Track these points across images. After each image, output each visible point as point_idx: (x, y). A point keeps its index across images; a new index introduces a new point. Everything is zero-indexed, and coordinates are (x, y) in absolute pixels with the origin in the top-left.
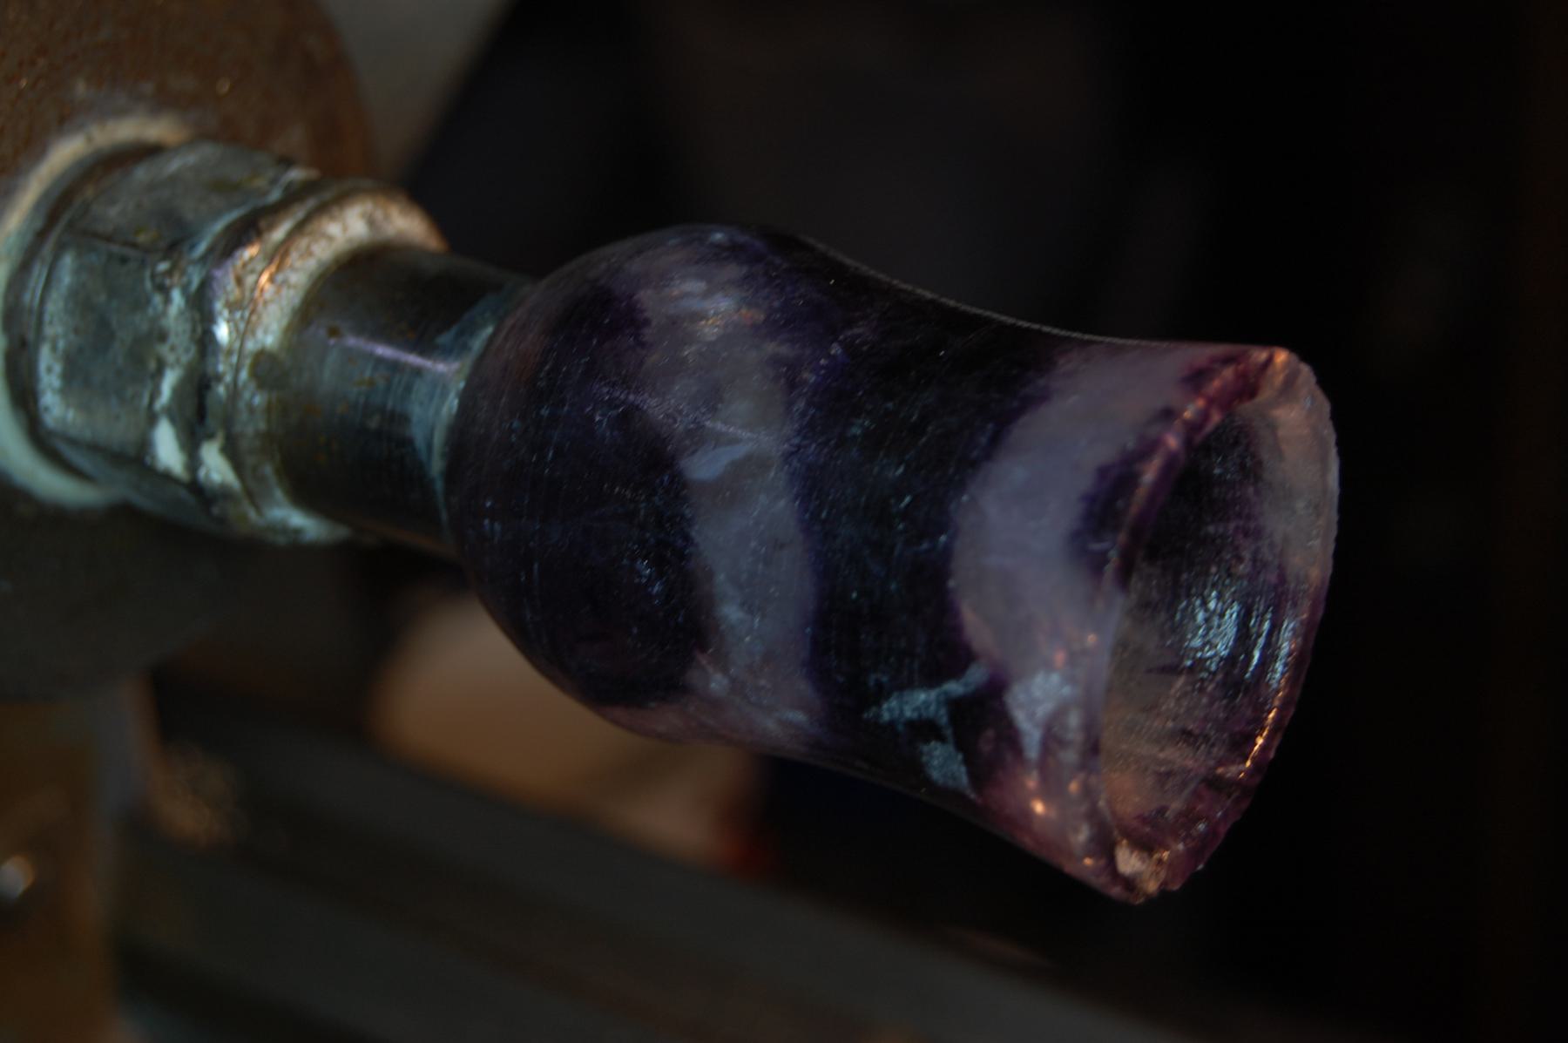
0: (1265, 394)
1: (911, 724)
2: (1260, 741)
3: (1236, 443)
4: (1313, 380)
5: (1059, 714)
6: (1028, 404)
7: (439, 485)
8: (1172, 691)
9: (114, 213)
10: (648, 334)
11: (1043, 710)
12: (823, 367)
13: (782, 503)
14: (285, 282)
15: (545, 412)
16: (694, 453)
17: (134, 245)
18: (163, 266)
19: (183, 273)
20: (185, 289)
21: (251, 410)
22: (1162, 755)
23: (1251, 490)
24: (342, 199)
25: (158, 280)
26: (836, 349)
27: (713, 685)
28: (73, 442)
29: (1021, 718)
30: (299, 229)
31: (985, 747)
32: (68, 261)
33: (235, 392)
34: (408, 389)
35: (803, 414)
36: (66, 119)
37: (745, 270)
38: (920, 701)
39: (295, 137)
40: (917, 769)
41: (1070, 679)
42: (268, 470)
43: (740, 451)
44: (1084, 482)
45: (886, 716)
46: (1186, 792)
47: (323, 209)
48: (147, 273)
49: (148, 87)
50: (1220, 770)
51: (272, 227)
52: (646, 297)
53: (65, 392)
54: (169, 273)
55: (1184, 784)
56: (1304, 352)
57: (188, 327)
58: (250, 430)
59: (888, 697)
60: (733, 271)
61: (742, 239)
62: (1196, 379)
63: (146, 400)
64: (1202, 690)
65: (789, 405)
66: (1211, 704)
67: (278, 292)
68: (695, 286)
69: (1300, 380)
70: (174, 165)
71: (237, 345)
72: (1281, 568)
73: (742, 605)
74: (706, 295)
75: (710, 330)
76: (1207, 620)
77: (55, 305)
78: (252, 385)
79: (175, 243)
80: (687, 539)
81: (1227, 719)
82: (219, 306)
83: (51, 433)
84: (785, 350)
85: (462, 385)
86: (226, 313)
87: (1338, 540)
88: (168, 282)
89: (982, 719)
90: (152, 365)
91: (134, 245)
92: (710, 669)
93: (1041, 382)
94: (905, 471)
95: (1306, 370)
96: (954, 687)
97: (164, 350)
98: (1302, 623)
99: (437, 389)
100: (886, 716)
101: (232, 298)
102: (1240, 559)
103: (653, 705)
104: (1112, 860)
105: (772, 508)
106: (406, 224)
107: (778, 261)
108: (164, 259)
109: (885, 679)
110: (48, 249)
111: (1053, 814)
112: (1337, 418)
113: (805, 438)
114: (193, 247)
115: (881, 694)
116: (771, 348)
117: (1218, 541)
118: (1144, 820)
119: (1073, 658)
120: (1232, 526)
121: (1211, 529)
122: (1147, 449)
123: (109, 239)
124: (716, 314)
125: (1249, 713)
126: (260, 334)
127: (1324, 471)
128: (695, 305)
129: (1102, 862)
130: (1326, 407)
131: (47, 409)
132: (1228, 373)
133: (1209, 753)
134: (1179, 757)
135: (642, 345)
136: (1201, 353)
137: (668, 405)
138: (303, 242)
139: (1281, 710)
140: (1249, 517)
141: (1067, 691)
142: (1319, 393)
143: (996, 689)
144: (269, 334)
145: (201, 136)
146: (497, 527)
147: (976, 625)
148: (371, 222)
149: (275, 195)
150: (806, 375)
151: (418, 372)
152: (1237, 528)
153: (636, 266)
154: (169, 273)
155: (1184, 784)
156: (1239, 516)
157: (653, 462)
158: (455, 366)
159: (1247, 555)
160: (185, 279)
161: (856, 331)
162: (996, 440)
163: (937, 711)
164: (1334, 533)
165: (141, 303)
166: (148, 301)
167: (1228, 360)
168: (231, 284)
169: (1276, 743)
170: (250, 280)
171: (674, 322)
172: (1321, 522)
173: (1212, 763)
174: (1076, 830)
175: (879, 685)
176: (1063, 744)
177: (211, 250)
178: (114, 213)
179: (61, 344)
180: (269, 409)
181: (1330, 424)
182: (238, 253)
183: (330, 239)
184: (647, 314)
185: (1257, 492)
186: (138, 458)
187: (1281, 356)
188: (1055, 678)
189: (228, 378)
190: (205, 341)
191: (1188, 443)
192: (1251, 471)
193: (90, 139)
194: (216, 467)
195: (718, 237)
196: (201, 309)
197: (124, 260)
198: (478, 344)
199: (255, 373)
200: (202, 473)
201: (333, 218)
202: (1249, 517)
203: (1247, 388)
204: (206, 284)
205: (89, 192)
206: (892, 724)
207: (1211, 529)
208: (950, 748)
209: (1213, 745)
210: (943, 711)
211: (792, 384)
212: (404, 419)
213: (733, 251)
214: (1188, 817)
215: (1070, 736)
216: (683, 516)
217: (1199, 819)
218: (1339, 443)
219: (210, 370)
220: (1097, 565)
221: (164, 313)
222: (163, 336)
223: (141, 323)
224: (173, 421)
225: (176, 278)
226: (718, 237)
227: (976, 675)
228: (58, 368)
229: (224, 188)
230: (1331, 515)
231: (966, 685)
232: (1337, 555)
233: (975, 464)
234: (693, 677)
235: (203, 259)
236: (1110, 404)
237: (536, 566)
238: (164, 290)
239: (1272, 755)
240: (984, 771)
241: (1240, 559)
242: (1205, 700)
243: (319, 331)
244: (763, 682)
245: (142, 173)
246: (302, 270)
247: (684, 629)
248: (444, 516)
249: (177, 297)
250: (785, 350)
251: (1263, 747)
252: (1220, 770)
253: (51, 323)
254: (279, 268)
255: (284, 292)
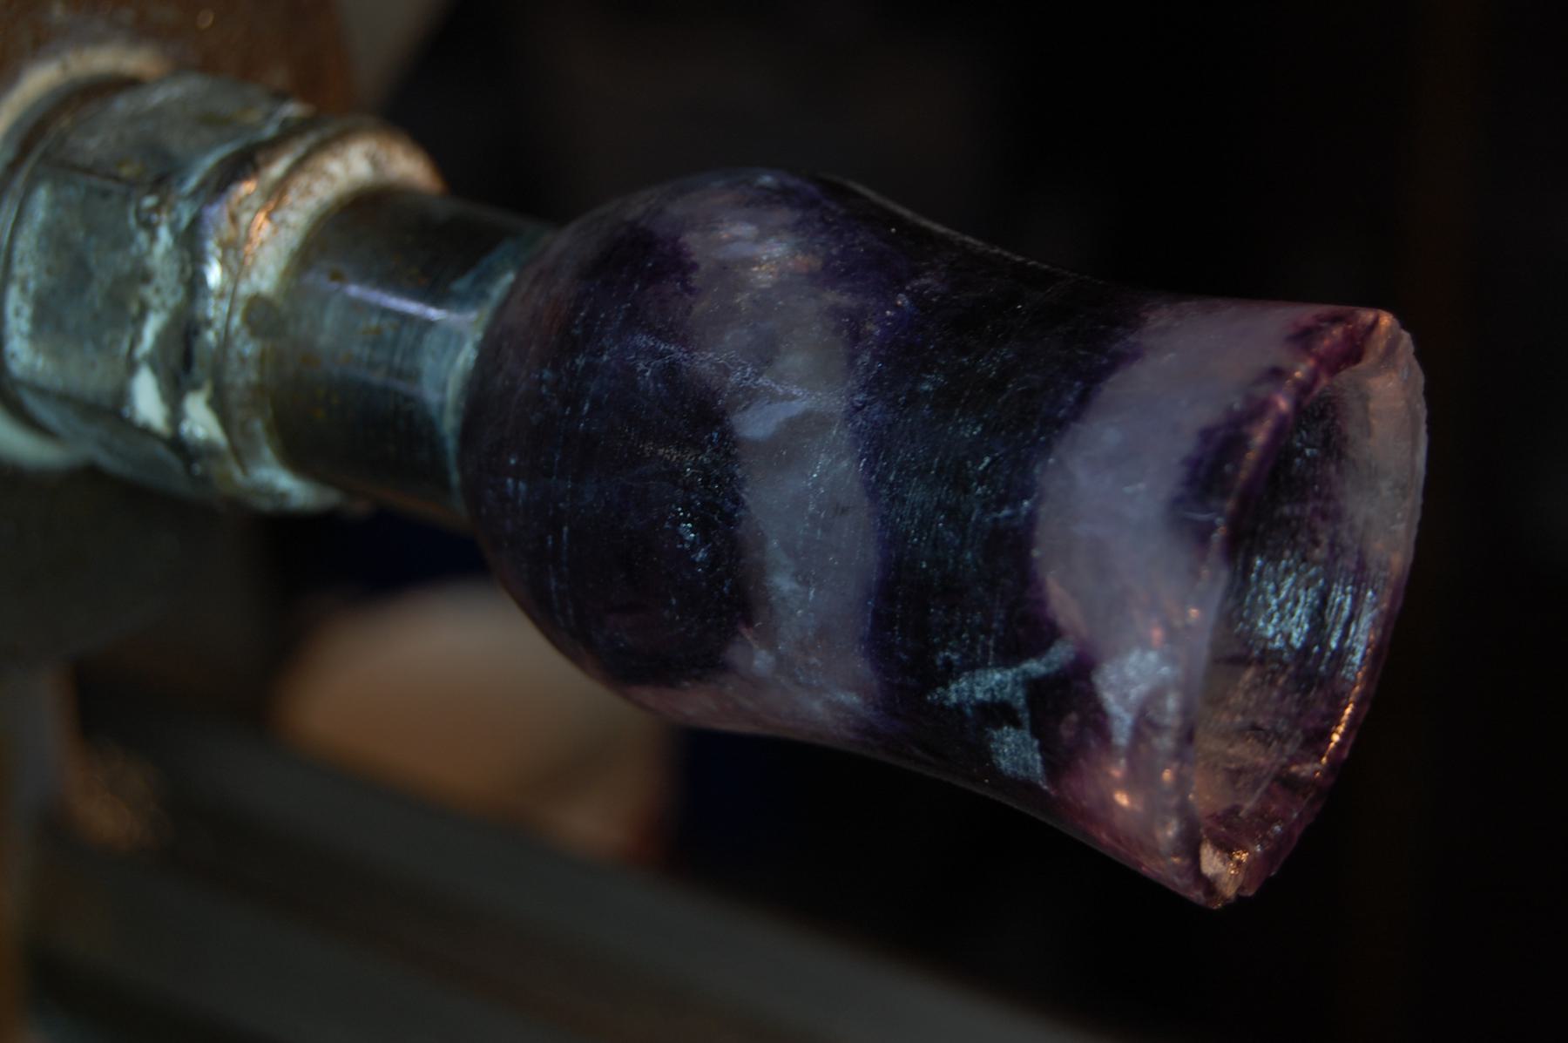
0: (1370, 359)
1: (981, 707)
2: (1336, 738)
3: (1323, 416)
4: (1412, 349)
5: (1156, 695)
6: (1118, 361)
7: (451, 445)
8: (1241, 684)
9: (92, 145)
10: (696, 279)
11: (1136, 692)
12: (888, 319)
13: (845, 464)
14: (283, 222)
15: (580, 362)
16: (746, 408)
17: (117, 179)
18: (149, 201)
19: (172, 209)
20: (173, 227)
21: (243, 360)
22: (1231, 751)
23: (1332, 468)
24: (343, 137)
25: (144, 216)
26: (902, 300)
27: (756, 663)
28: (42, 392)
29: (1110, 700)
30: (298, 166)
31: (1066, 732)
32: (42, 195)
33: (226, 339)
34: (419, 339)
35: (868, 369)
36: (41, 44)
37: (798, 215)
38: (994, 682)
39: (279, 77)
40: (982, 755)
41: (1170, 659)
42: (258, 426)
43: (797, 408)
44: (1187, 445)
45: (954, 698)
46: (1259, 791)
47: (324, 146)
48: (132, 210)
49: (127, 15)
50: (1294, 769)
51: (269, 162)
52: (693, 241)
53: (34, 337)
54: (156, 209)
55: (1256, 783)
56: (1405, 321)
57: (176, 267)
58: (240, 381)
59: (959, 675)
60: (784, 215)
61: (792, 182)
62: (1303, 338)
63: (126, 345)
64: (1273, 683)
65: (853, 358)
66: (1283, 697)
67: (275, 232)
68: (746, 230)
69: (1400, 348)
70: (158, 97)
71: (229, 288)
72: (1361, 553)
73: (795, 575)
74: (760, 239)
75: (763, 277)
76: (1281, 606)
77: (26, 243)
78: (244, 333)
79: (163, 178)
80: (737, 501)
81: (1300, 714)
82: (211, 245)
83: (17, 383)
84: (846, 300)
85: (479, 336)
86: (219, 252)
87: (1421, 525)
88: (155, 217)
89: (1065, 704)
90: (134, 308)
91: (117, 179)
92: (756, 646)
93: (1132, 339)
94: (984, 429)
95: (1406, 337)
96: (1035, 667)
97: (148, 292)
98: (1381, 613)
99: (448, 345)
100: (954, 698)
101: (226, 236)
102: (1316, 543)
103: (687, 684)
104: (1196, 858)
105: (832, 468)
106: (408, 167)
107: (833, 207)
108: (150, 193)
109: (955, 657)
110: (19, 182)
111: (1139, 808)
112: (1430, 394)
113: (870, 394)
114: (182, 181)
115: (950, 673)
116: (831, 297)
117: (1294, 523)
118: (1213, 816)
119: (1172, 634)
120: (1309, 508)
121: (1286, 510)
122: (1258, 410)
123: (89, 171)
124: (769, 260)
125: (1323, 708)
126: (255, 277)
127: (1415, 447)
128: (743, 250)
129: (1187, 862)
130: (1421, 380)
131: (13, 355)
132: (1337, 332)
133: (1282, 750)
134: (1245, 751)
135: (691, 291)
136: (1306, 313)
137: (717, 358)
138: (302, 180)
139: (1357, 705)
140: (1329, 498)
141: (1165, 670)
142: (1415, 363)
143: (1082, 670)
144: (266, 272)
145: (179, 69)
146: (522, 486)
147: (1062, 599)
148: (374, 162)
149: (270, 131)
150: (870, 327)
151: (429, 324)
152: (1315, 510)
153: (677, 209)
154: (156, 209)
155: (1256, 783)
156: (1318, 496)
157: (703, 415)
158: (472, 316)
159: (1324, 539)
160: (174, 216)
161: (924, 281)
162: (1084, 400)
163: (1013, 694)
164: (1417, 517)
165: (123, 241)
166: (131, 239)
167: (1335, 320)
168: (225, 225)
169: (1351, 741)
170: (245, 218)
171: (724, 268)
172: (1408, 504)
173: (1284, 760)
174: (1165, 824)
175: (948, 663)
176: (1157, 728)
177: (203, 184)
178: (92, 145)
179: (32, 285)
180: (262, 359)
181: (1422, 399)
182: (233, 188)
183: (331, 178)
184: (693, 258)
185: (1339, 471)
186: (111, 410)
187: (1386, 320)
188: (1152, 657)
189: (219, 325)
190: (194, 284)
191: (1297, 405)
192: (1334, 446)
193: (65, 67)
194: (200, 421)
195: (767, 180)
196: (191, 244)
197: (106, 194)
198: (498, 291)
199: (248, 320)
200: (185, 428)
201: (335, 156)
202: (1329, 498)
203: (1352, 352)
204: (196, 222)
205: (65, 122)
206: (959, 706)
207: (1286, 510)
208: (1027, 734)
209: (1285, 742)
210: (1020, 694)
211: (856, 337)
212: (414, 376)
213: (784, 196)
214: (1263, 818)
215: (1168, 721)
216: (732, 476)
217: (1273, 821)
218: (1430, 421)
219: (199, 314)
220: (1202, 535)
221: (150, 252)
222: (146, 277)
223: (122, 263)
224: (155, 370)
225: (164, 217)
226: (767, 180)
227: (1060, 654)
228: (27, 311)
229: (214, 122)
230: (1415, 500)
231: (1048, 665)
232: (1419, 543)
233: (1061, 424)
234: (735, 654)
235: (194, 194)
236: (1198, 366)
237: (566, 529)
238: (151, 228)
239: (1346, 754)
240: (1060, 760)
241: (1316, 543)
242: (1275, 694)
243: (310, 278)
244: (813, 660)
245: (122, 105)
246: (301, 210)
247: (727, 600)
248: (455, 478)
249: (164, 235)
250: (846, 300)
251: (1339, 745)
252: (1294, 769)
253: (21, 261)
254: (277, 207)
255: (283, 232)
